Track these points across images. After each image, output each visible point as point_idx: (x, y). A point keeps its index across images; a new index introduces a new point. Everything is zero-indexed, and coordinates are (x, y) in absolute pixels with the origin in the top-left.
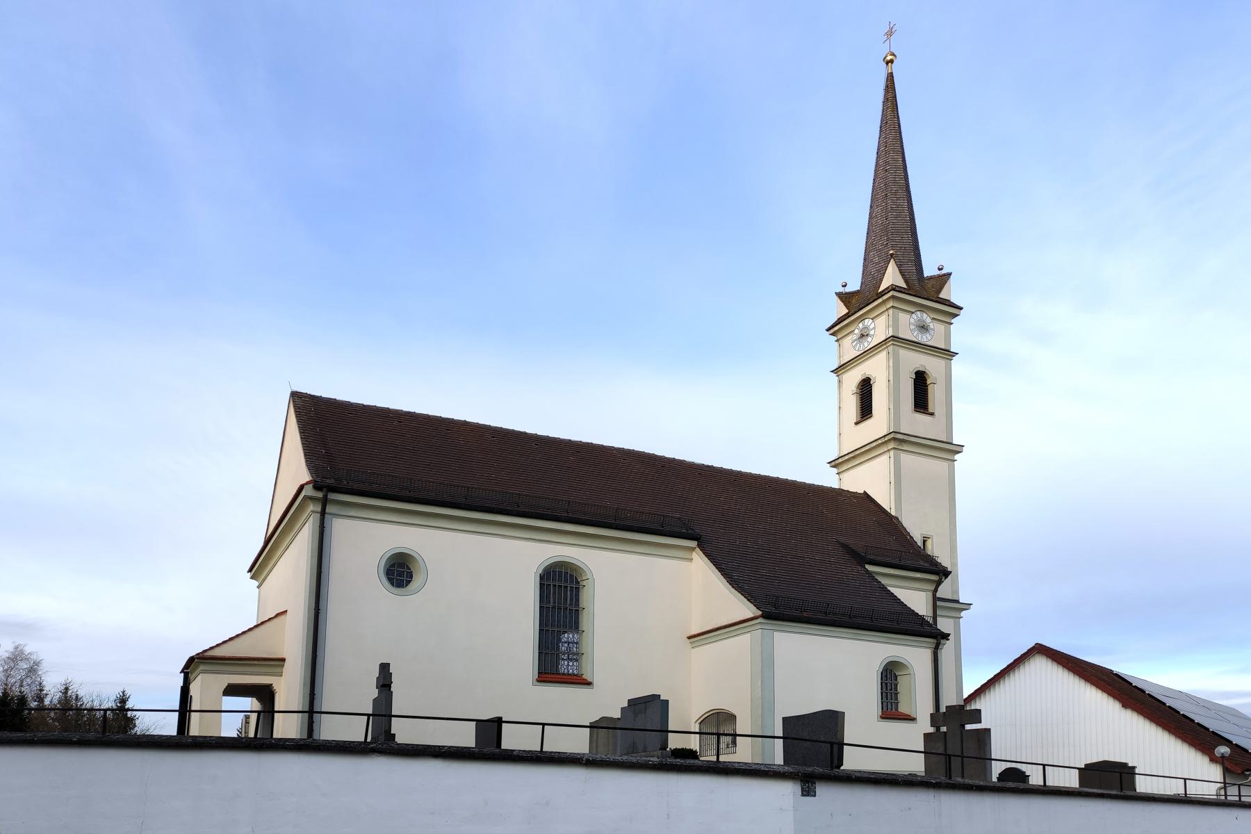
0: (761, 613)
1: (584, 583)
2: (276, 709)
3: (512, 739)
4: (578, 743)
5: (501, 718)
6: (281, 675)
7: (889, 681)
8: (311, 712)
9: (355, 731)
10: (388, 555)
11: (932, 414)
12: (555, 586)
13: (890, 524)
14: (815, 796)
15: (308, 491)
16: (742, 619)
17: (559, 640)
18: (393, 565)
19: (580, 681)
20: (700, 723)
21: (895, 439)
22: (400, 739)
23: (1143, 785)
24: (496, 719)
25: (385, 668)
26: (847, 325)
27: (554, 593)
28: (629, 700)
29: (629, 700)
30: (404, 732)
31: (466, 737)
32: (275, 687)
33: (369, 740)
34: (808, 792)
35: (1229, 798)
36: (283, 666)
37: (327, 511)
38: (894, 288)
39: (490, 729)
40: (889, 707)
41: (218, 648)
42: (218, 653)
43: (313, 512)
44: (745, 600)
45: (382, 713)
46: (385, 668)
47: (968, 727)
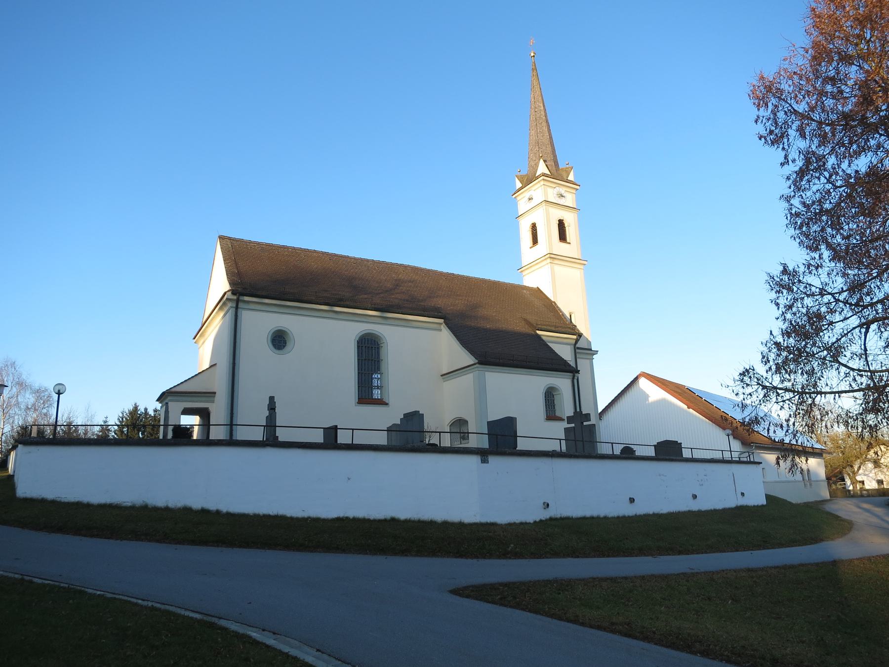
0: (477, 361)
1: (382, 345)
2: (211, 424)
3: (343, 438)
4: (381, 439)
5: (337, 426)
6: (214, 402)
7: (549, 399)
8: (231, 425)
9: (258, 435)
10: (273, 331)
11: (569, 243)
12: (366, 347)
13: (551, 307)
14: (488, 463)
15: (229, 295)
16: (468, 365)
17: (372, 379)
18: (276, 337)
19: (381, 402)
20: (450, 426)
21: (550, 258)
22: (280, 439)
23: (686, 454)
24: (334, 427)
25: (272, 399)
26: (522, 193)
27: (366, 352)
28: (404, 414)
29: (404, 414)
30: (283, 435)
31: (318, 437)
32: (210, 409)
33: (265, 439)
34: (484, 461)
35: (733, 459)
36: (215, 396)
37: (239, 306)
38: (544, 175)
39: (331, 432)
40: (551, 413)
41: (175, 388)
42: (178, 389)
43: (231, 307)
44: (469, 354)
45: (271, 425)
46: (272, 399)
47: (585, 423)
